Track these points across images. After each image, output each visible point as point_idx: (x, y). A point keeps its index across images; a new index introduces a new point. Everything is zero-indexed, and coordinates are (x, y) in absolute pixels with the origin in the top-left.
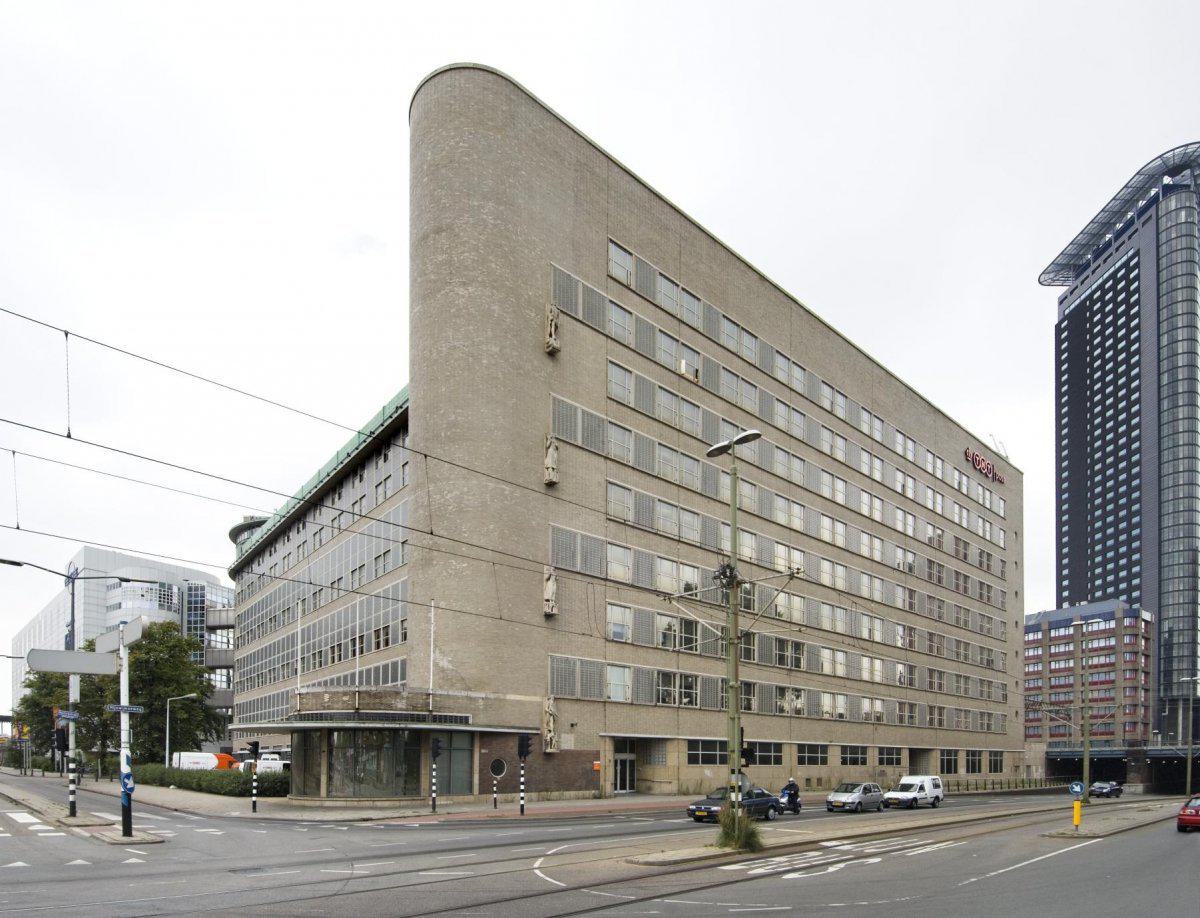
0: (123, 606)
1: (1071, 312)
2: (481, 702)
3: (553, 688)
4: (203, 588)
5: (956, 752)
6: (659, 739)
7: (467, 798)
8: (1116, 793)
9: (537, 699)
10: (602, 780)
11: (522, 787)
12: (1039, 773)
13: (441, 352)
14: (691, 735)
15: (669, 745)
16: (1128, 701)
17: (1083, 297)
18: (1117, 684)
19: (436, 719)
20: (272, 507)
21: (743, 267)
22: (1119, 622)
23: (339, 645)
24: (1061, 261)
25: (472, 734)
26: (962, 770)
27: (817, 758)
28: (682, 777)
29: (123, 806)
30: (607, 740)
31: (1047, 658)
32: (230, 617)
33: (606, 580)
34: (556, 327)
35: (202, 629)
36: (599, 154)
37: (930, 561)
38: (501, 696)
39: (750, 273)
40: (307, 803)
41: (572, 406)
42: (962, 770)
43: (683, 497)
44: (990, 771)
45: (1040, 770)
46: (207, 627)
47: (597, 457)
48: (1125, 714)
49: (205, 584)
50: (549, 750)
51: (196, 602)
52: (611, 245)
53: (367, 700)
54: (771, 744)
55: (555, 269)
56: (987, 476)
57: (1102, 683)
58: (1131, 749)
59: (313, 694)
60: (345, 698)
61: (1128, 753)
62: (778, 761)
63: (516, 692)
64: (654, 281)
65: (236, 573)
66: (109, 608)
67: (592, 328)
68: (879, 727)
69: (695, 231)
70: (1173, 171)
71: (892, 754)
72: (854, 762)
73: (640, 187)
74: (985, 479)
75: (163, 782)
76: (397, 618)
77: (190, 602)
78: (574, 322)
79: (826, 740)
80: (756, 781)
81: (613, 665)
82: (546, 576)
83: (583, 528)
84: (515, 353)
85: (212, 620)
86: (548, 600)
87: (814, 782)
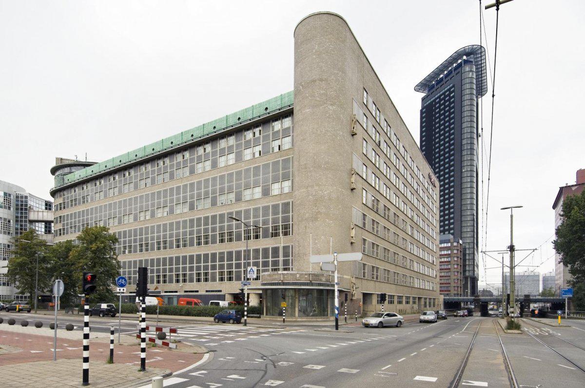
1: (427, 105)
4: (26, 197)
6: (369, 294)
8: (260, 317)
11: (284, 314)
17: (432, 100)
18: (451, 270)
22: (452, 244)
23: (64, 229)
24: (423, 82)
35: (26, 221)
40: (274, 319)
44: (378, 303)
46: (29, 221)
53: (314, 277)
57: (445, 269)
60: (306, 276)
70: (468, 54)
76: (106, 217)
86: (352, 237)
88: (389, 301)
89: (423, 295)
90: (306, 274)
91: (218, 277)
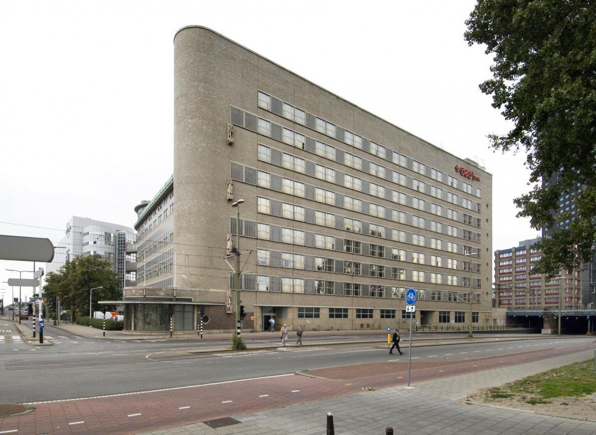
0: (89, 244)
2: (198, 293)
3: (231, 286)
5: (449, 313)
6: (430, 311)
7: (191, 332)
9: (224, 291)
10: (255, 324)
12: (501, 322)
13: (183, 147)
14: (299, 305)
15: (288, 309)
16: (567, 286)
19: (177, 300)
20: (151, 197)
21: (327, 94)
25: (194, 305)
26: (452, 321)
27: (367, 315)
28: (295, 324)
29: (40, 333)
30: (258, 308)
31: (514, 266)
32: (135, 247)
33: (257, 239)
34: (232, 133)
36: (253, 54)
37: (465, 215)
38: (207, 290)
39: (331, 96)
41: (240, 165)
42: (452, 321)
43: (295, 201)
44: (440, 322)
45: (502, 321)
47: (253, 187)
48: (566, 293)
49: (125, 232)
50: (228, 312)
51: (122, 241)
52: (259, 93)
54: (342, 309)
55: (232, 107)
56: (469, 178)
58: (545, 311)
59: (129, 290)
60: (141, 291)
61: (544, 314)
62: (346, 316)
63: (214, 288)
64: (272, 108)
65: (137, 227)
66: (84, 245)
67: (250, 131)
68: (402, 301)
69: (302, 81)
71: (384, 313)
72: (388, 317)
73: (273, 66)
74: (467, 179)
75: (87, 324)
77: (119, 241)
78: (241, 129)
79: (372, 307)
80: (333, 325)
81: (260, 275)
82: (228, 239)
83: (246, 217)
84: (213, 146)
85: (129, 249)
86: (228, 249)
87: (365, 326)
88: (440, 317)
89: (437, 309)
90: (140, 290)
91: (125, 264)
